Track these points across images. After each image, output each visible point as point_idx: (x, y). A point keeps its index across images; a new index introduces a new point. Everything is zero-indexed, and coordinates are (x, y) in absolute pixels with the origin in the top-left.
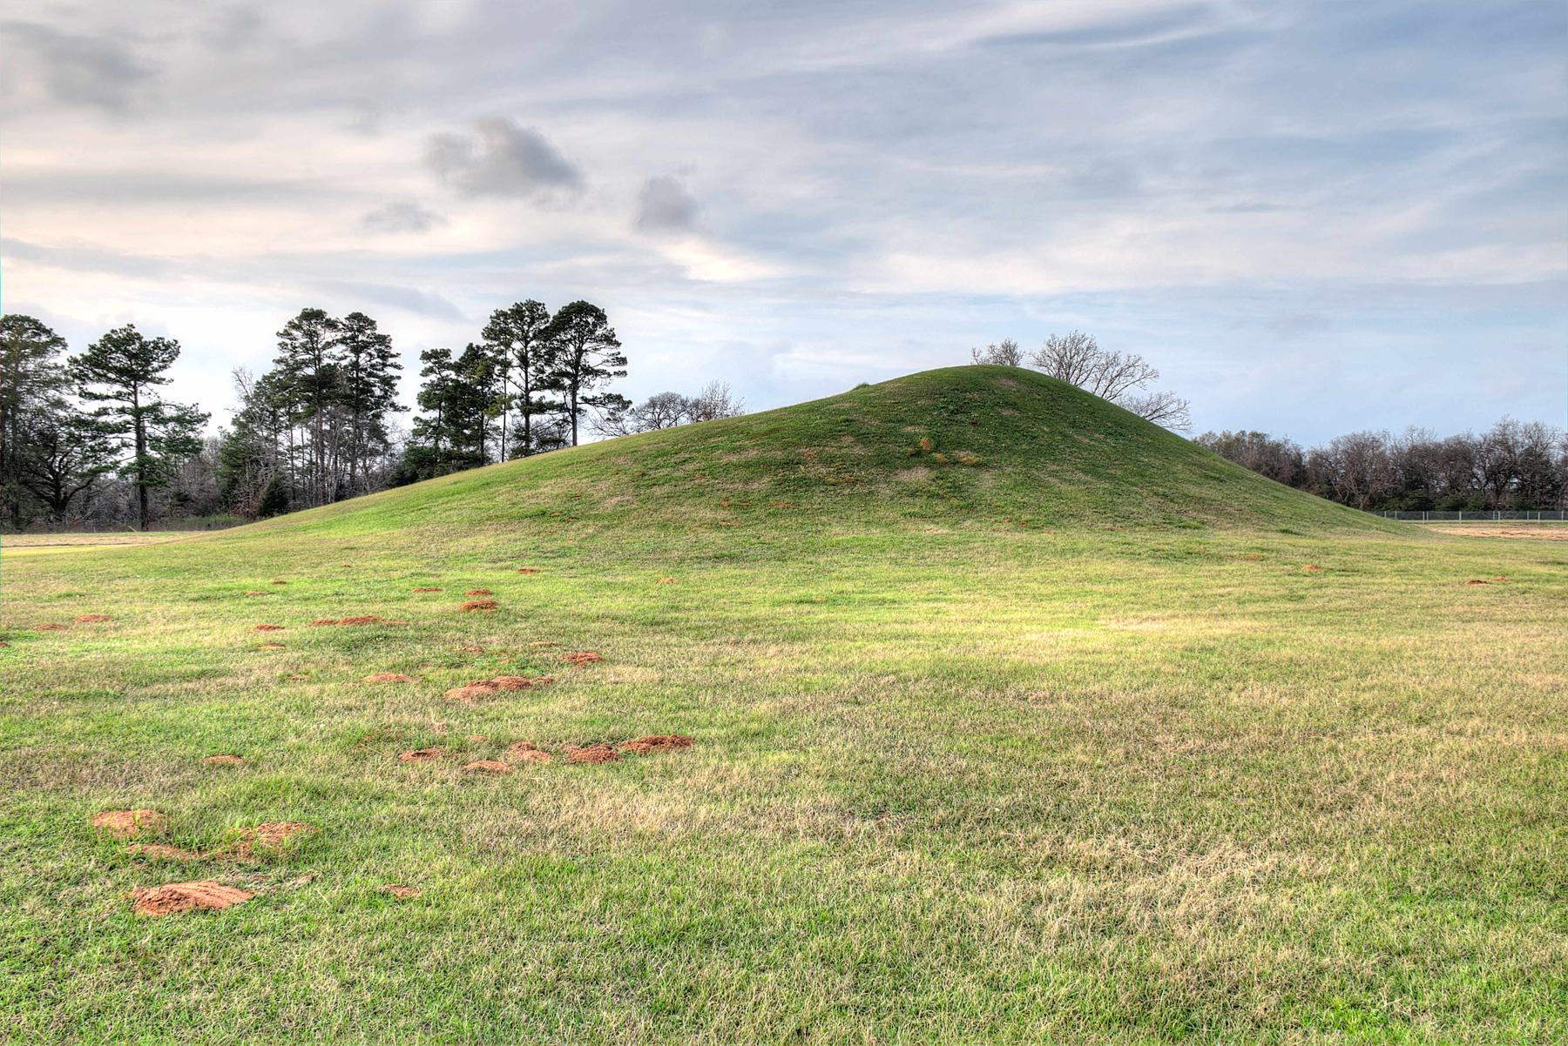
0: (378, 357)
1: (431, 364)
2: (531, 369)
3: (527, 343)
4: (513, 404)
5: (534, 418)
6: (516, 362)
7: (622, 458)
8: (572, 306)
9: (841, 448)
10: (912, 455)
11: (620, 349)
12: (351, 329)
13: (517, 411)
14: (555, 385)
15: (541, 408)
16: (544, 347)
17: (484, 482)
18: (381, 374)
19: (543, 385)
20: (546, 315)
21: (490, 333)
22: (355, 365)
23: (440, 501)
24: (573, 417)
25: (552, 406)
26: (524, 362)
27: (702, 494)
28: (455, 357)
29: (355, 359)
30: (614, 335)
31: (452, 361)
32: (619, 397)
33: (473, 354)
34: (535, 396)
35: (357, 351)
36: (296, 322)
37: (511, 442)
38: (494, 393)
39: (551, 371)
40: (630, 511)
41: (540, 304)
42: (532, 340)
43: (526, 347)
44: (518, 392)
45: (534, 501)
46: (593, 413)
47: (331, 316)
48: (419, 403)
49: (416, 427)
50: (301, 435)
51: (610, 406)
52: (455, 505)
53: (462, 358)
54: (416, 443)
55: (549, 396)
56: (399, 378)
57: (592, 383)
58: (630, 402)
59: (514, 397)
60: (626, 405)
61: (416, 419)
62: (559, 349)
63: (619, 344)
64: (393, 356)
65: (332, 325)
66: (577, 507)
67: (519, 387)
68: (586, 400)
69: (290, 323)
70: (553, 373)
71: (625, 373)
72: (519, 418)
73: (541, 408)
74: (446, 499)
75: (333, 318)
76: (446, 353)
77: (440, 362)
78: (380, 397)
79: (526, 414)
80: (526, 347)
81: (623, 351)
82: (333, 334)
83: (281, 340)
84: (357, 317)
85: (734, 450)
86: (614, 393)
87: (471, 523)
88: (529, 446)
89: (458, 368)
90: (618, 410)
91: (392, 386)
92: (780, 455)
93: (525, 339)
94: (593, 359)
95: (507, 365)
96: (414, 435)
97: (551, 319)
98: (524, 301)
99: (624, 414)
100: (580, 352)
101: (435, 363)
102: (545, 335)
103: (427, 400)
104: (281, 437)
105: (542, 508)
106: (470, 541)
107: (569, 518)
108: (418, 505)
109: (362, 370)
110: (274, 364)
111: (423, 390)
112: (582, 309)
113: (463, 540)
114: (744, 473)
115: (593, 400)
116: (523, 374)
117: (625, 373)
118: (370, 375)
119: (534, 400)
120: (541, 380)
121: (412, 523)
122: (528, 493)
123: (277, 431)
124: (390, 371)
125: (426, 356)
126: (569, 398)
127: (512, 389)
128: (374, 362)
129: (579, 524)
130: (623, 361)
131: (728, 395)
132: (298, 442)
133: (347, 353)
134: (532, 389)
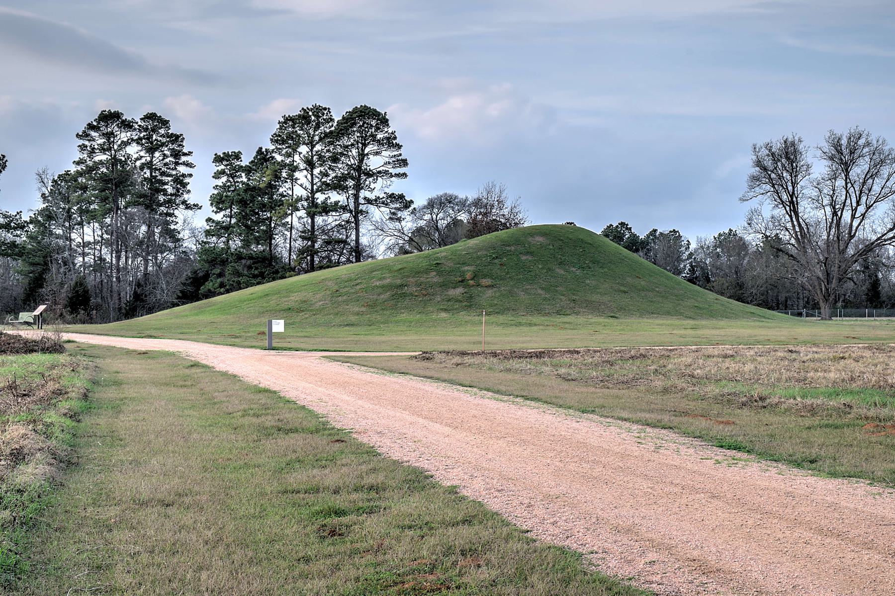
0: (171, 155)
1: (223, 167)
2: (316, 171)
3: (313, 146)
4: (299, 205)
5: (319, 220)
6: (302, 165)
7: (331, 282)
8: (355, 110)
9: (427, 278)
10: (459, 282)
11: (402, 151)
12: (146, 129)
13: (302, 213)
14: (338, 185)
15: (326, 209)
16: (328, 151)
17: (266, 293)
18: (174, 173)
19: (327, 187)
20: (332, 120)
21: (277, 139)
22: (149, 165)
23: (245, 303)
24: (356, 217)
25: (336, 207)
26: (310, 164)
27: (358, 301)
28: (245, 161)
29: (149, 159)
30: (395, 138)
31: (243, 164)
32: (401, 197)
33: (263, 158)
34: (320, 197)
35: (151, 150)
36: (95, 123)
37: (298, 242)
38: (282, 195)
39: (334, 175)
40: (326, 308)
41: (325, 109)
42: (317, 143)
43: (311, 150)
44: (304, 193)
45: (286, 303)
46: (378, 214)
47: (127, 117)
48: (212, 204)
49: (208, 228)
50: (90, 232)
51: (392, 206)
52: (252, 305)
53: (252, 162)
54: (208, 243)
55: (335, 197)
56: (191, 175)
57: (372, 186)
58: (412, 202)
59: (300, 199)
60: (407, 205)
61: (209, 220)
62: (342, 154)
63: (399, 147)
64: (185, 154)
65: (127, 125)
66: (304, 306)
67: (306, 189)
68: (369, 201)
69: (89, 124)
70: (336, 177)
71: (404, 175)
72: (305, 220)
73: (326, 209)
74: (248, 302)
75: (129, 119)
76: (237, 156)
77: (231, 164)
78: (171, 195)
79: (312, 215)
80: (311, 150)
81: (405, 153)
82: (129, 134)
83: (81, 142)
84: (151, 117)
85: (380, 279)
86: (397, 192)
87: (259, 313)
88: (314, 246)
89: (248, 170)
90: (399, 209)
91: (184, 185)
92: (399, 282)
93: (312, 144)
94: (374, 163)
95: (294, 169)
96: (206, 236)
97: (335, 124)
98: (310, 107)
99: (405, 214)
100: (362, 156)
101: (226, 166)
102: (331, 137)
103: (219, 202)
104: (73, 236)
105: (290, 307)
106: (259, 320)
107: (300, 311)
108: (235, 305)
109: (156, 169)
110: (74, 166)
111: (216, 192)
112: (364, 113)
113: (255, 320)
114: (380, 290)
115: (376, 200)
116: (309, 177)
117: (404, 175)
118: (163, 174)
119: (319, 201)
120: (325, 183)
121: (234, 313)
122: (285, 299)
123: (71, 228)
124: (182, 169)
125: (218, 159)
126: (351, 201)
127: (299, 192)
128: (167, 160)
129: (303, 313)
130: (404, 163)
131: (504, 195)
132: (89, 238)
133: (142, 153)
134: (318, 191)
